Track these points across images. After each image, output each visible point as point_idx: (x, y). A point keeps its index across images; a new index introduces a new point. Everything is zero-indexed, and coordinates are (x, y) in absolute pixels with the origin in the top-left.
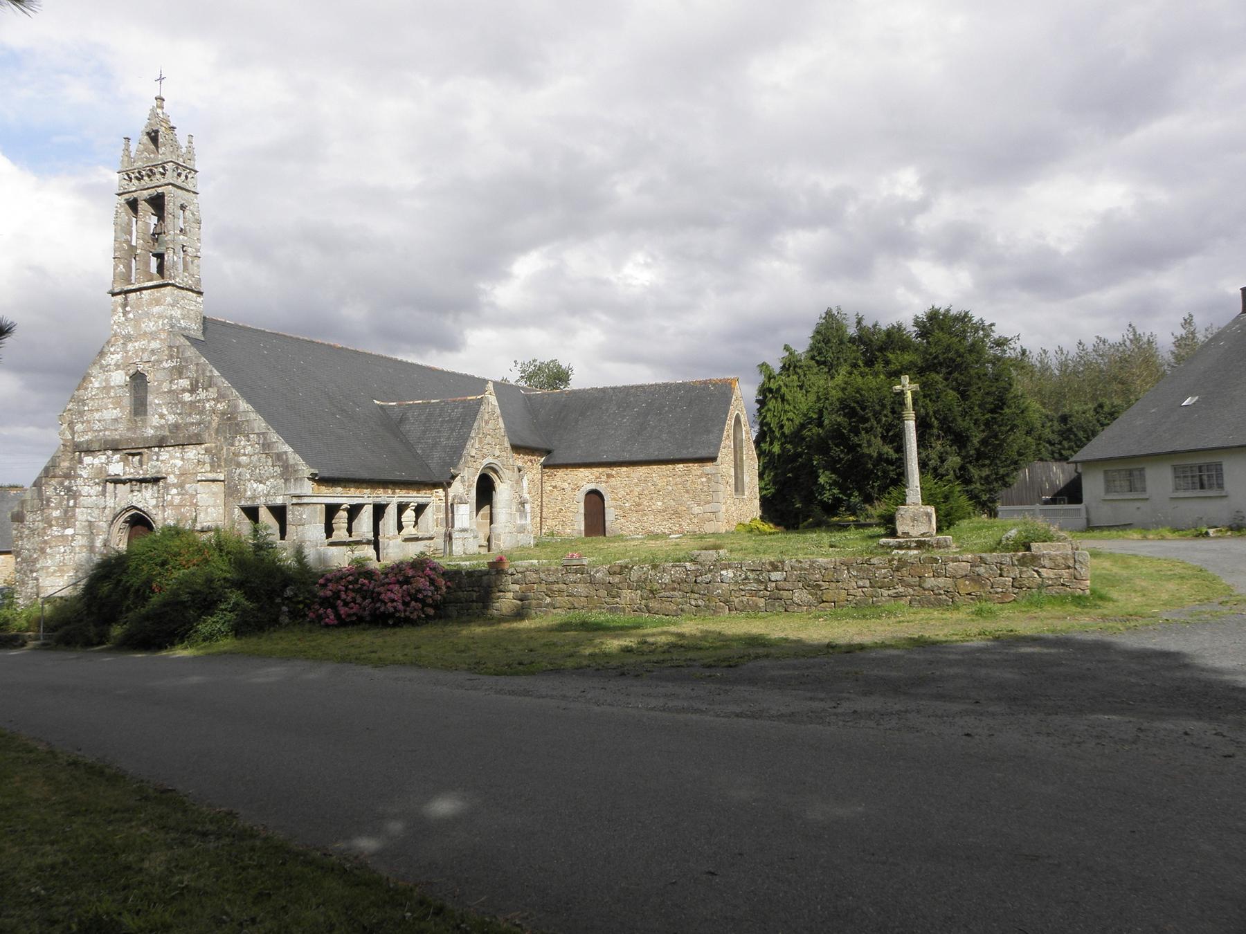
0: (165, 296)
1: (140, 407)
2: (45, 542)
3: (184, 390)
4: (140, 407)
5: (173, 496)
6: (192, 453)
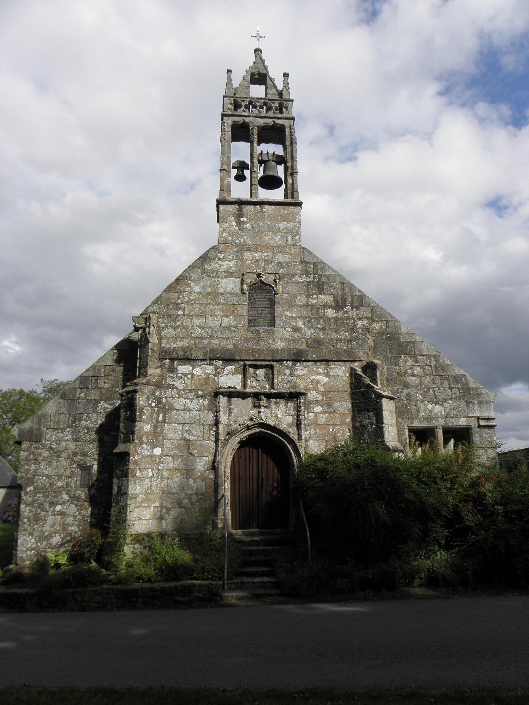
3: (326, 306)
5: (316, 414)
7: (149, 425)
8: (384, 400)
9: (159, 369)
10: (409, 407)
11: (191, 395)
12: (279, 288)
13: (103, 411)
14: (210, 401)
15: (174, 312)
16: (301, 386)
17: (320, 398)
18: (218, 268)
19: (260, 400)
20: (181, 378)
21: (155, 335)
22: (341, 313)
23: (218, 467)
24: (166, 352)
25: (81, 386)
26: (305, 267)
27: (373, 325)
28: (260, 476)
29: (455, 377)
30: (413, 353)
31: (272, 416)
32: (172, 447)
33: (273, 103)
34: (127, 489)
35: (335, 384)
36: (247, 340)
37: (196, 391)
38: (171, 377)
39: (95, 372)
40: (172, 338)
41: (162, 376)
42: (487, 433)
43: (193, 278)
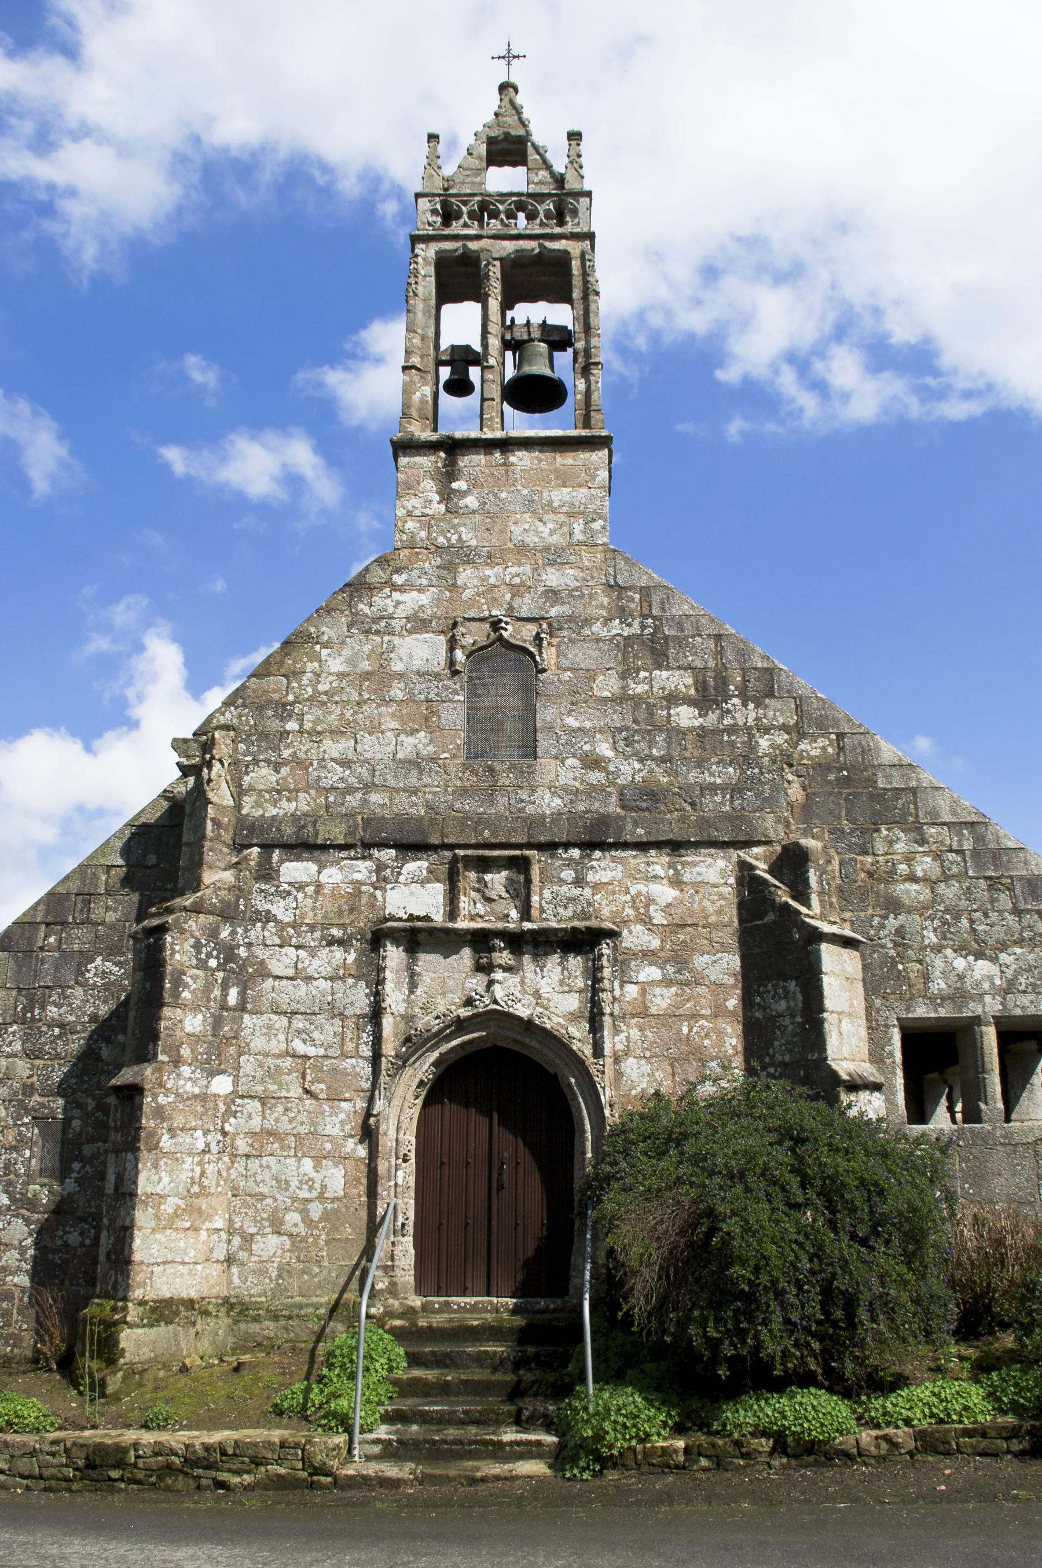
3: (673, 699)
7: (200, 1017)
8: (825, 948)
9: (231, 871)
10: (900, 967)
11: (309, 939)
12: (549, 657)
13: (99, 982)
14: (361, 953)
15: (275, 725)
16: (605, 912)
17: (656, 943)
18: (391, 610)
19: (492, 949)
20: (289, 893)
21: (224, 785)
22: (713, 717)
23: (377, 1127)
24: (252, 828)
25: (50, 919)
26: (619, 598)
27: (802, 747)
28: (495, 1154)
30: (911, 819)
31: (524, 992)
32: (259, 1074)
33: (541, 203)
34: (135, 1183)
35: (696, 906)
36: (462, 792)
37: (325, 927)
38: (262, 891)
39: (83, 882)
41: (239, 891)
43: (325, 638)
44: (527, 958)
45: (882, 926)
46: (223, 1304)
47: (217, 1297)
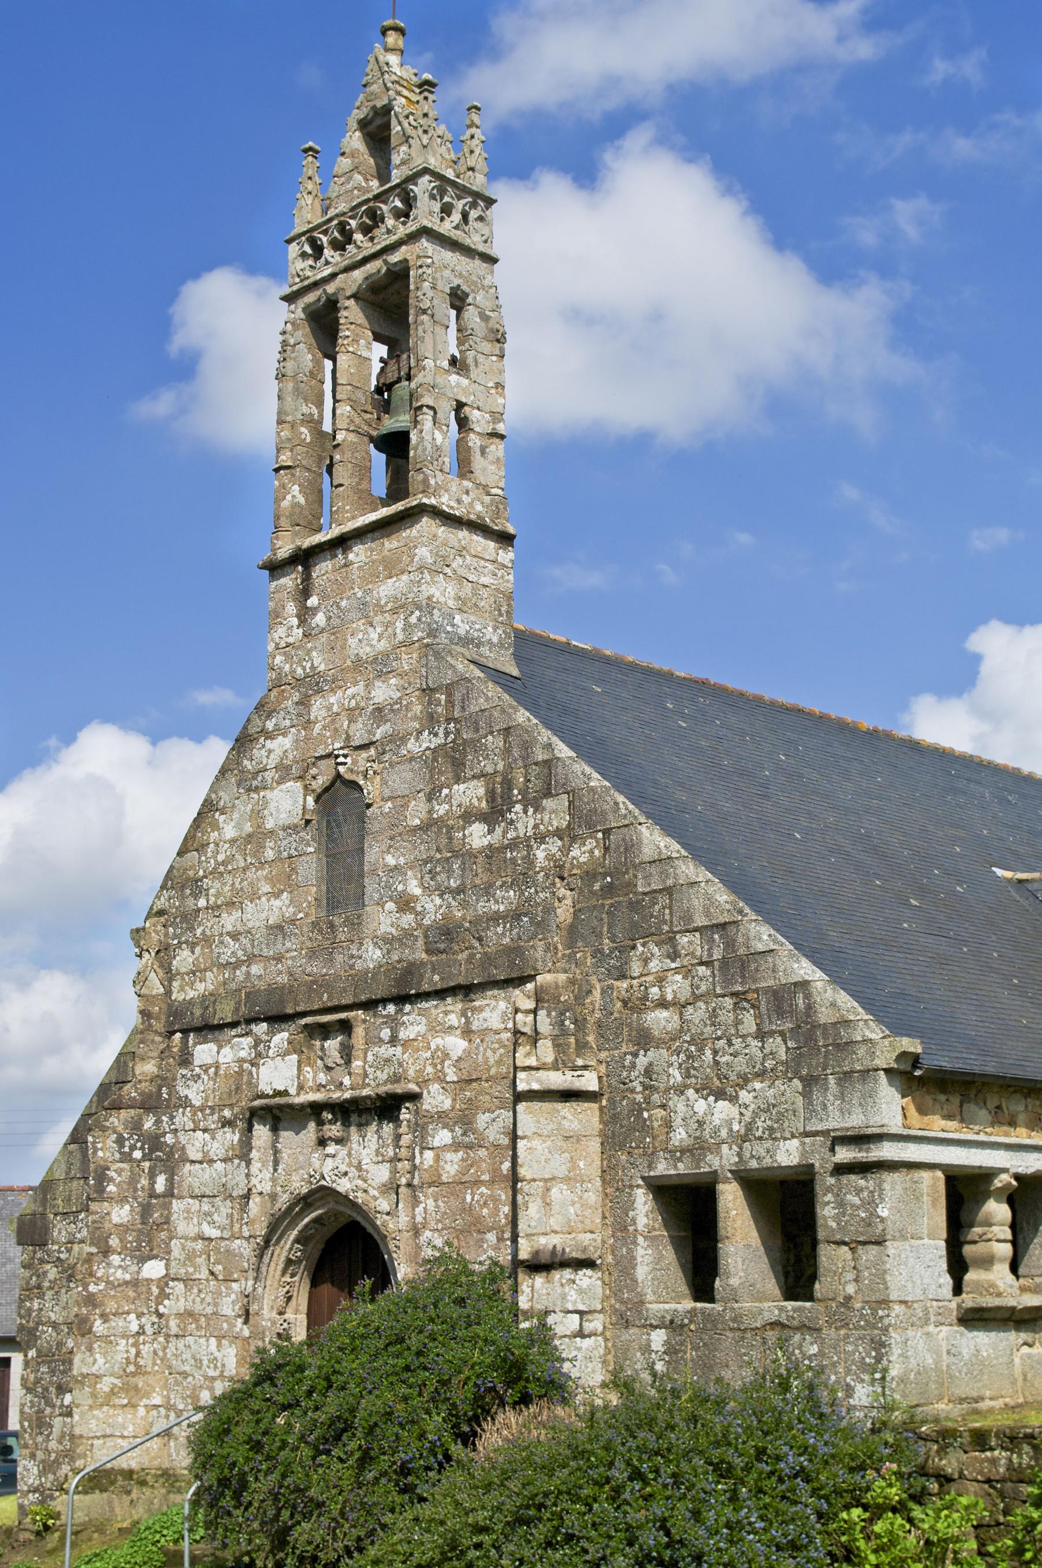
0: (410, 547)
1: (343, 887)
2: (91, 1300)
3: (469, 816)
4: (343, 887)
6: (493, 1011)
7: (127, 1207)
26: (430, 703)
29: (775, 993)
30: (666, 928)
35: (480, 1057)
40: (188, 974)
42: (859, 1191)
44: (353, 1129)
45: (633, 1066)
46: (162, 1476)
47: (158, 1469)
